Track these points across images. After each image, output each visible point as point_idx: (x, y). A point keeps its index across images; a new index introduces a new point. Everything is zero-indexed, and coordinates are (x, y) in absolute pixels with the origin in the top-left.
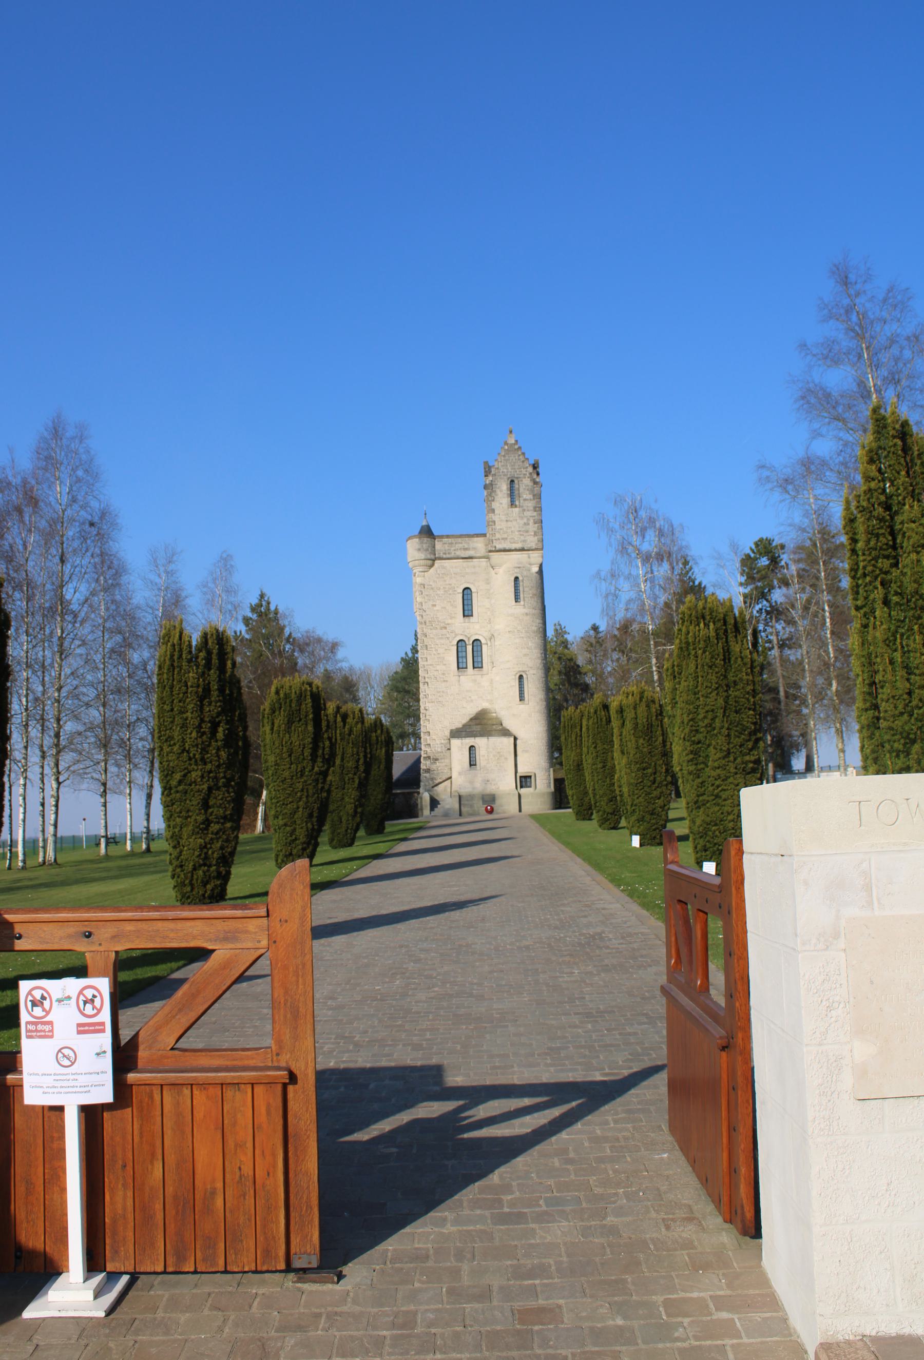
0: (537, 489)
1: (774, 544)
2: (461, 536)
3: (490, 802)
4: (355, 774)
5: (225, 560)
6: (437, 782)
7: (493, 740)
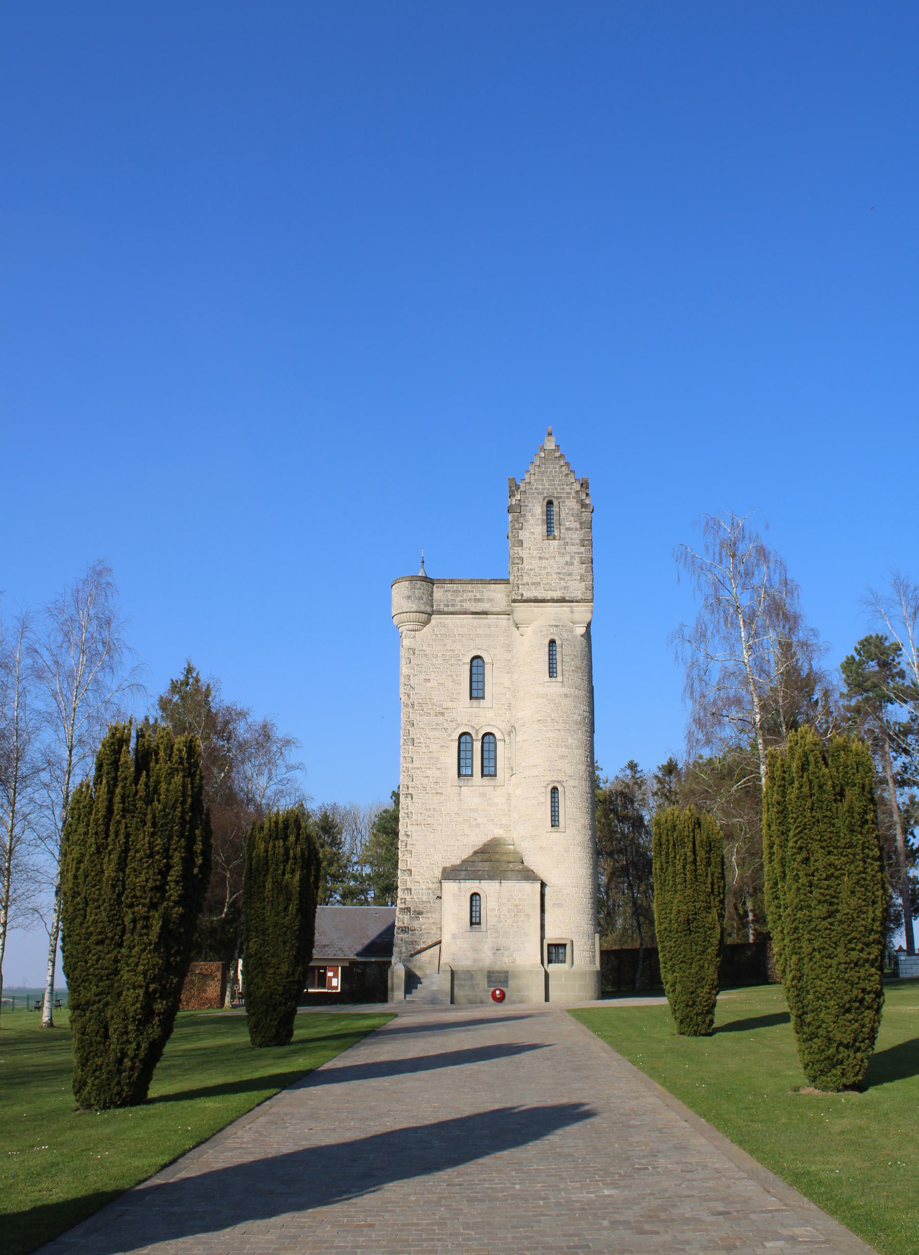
0: (586, 516)
1: (887, 644)
2: (471, 582)
3: (499, 984)
4: (153, 906)
5: (100, 574)
6: (418, 948)
7: (507, 884)
